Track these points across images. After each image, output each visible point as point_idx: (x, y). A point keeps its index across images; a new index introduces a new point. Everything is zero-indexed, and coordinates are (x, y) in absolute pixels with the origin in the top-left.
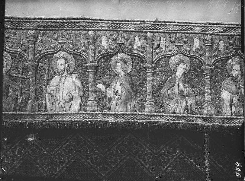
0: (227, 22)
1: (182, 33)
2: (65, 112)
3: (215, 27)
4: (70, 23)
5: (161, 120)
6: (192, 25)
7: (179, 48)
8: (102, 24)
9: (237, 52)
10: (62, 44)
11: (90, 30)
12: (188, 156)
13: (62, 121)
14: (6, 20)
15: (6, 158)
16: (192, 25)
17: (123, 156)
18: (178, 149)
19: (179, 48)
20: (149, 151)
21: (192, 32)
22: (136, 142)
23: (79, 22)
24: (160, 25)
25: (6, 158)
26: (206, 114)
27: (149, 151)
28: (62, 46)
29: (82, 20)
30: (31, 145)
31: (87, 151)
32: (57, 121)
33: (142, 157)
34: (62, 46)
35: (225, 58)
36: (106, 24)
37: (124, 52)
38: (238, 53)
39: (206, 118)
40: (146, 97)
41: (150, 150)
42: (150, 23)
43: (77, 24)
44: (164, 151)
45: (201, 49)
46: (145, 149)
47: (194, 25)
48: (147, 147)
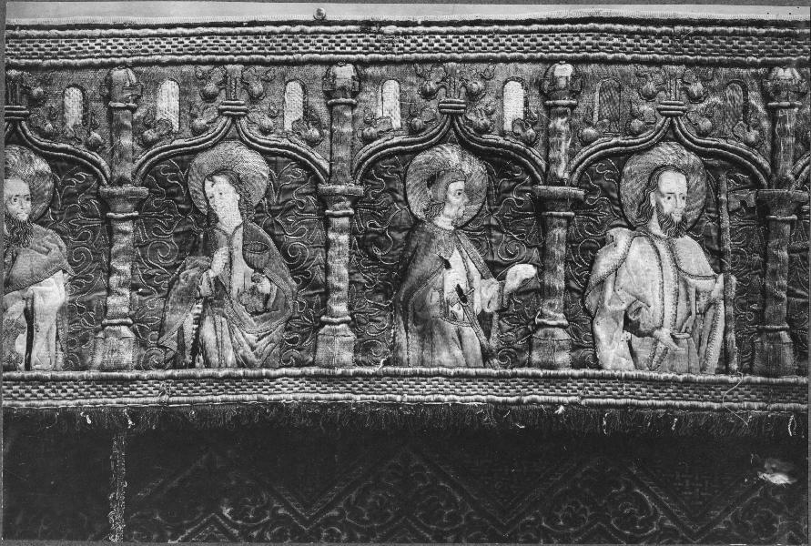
0: (536, 13)
1: (689, 64)
2: (654, 374)
3: (86, 37)
4: (645, 35)
5: (289, 394)
6: (173, 31)
7: (235, 119)
8: (557, 35)
9: (452, 125)
10: (671, 116)
11: (557, 61)
12: (430, 533)
13: (660, 407)
14: (807, 31)
15: (324, 534)
16: (173, 31)
17: (188, 526)
18: (226, 500)
19: (235, 119)
20: (668, 523)
21: (277, 58)
22: (623, 488)
23: (609, 31)
24: (312, 33)
25: (324, 534)
26: (102, 368)
27: (668, 523)
28: (672, 126)
29: (605, 23)
30: (616, 494)
31: (440, 515)
32: (681, 407)
33: (255, 534)
34: (672, 126)
35: (186, 148)
36: (522, 36)
37: (681, 143)
38: (18, 133)
39: (101, 380)
40: (350, 308)
41: (674, 519)
42: (344, 28)
43: (659, 42)
44: (727, 523)
45: (528, 119)
46: (656, 513)
47: (180, 30)
48: (665, 508)
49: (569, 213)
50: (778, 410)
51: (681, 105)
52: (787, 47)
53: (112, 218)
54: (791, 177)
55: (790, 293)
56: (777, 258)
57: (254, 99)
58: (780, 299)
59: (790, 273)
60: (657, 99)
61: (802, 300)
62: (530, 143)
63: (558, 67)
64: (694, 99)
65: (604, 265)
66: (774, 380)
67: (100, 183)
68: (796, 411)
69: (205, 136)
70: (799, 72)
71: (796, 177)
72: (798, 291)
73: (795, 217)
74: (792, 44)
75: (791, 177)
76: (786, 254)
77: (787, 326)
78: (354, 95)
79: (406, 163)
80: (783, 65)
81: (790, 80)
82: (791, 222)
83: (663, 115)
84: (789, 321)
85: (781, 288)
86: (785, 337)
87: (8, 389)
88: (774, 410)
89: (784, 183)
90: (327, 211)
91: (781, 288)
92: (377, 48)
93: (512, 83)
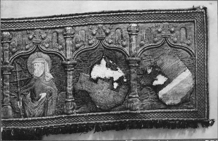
1: (41, 29)
11: (67, 26)
49: (72, 69)
50: (9, 128)
51: (168, 34)
52: (6, 26)
53: (4, 74)
54: (9, 62)
55: (10, 95)
56: (6, 85)
57: (107, 34)
58: (7, 96)
59: (10, 89)
60: (96, 35)
61: (14, 96)
62: (124, 46)
63: (67, 28)
64: (172, 32)
65: (135, 80)
66: (6, 120)
67: (62, 60)
68: (14, 128)
69: (93, 45)
70: (10, 33)
71: (10, 62)
72: (13, 94)
73: (10, 73)
74: (20, 24)
75: (9, 62)
76: (8, 84)
77: (10, 104)
78: (10, 39)
79: (27, 58)
80: (5, 31)
81: (7, 35)
82: (10, 75)
83: (163, 37)
84: (11, 102)
85: (8, 93)
86: (9, 107)
87: (109, 118)
88: (8, 128)
89: (6, 64)
90: (3, 73)
91: (8, 93)
92: (191, 18)
93: (183, 28)
